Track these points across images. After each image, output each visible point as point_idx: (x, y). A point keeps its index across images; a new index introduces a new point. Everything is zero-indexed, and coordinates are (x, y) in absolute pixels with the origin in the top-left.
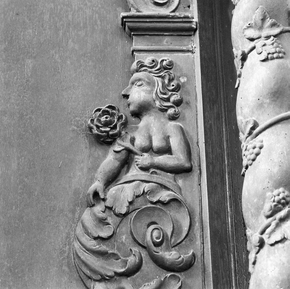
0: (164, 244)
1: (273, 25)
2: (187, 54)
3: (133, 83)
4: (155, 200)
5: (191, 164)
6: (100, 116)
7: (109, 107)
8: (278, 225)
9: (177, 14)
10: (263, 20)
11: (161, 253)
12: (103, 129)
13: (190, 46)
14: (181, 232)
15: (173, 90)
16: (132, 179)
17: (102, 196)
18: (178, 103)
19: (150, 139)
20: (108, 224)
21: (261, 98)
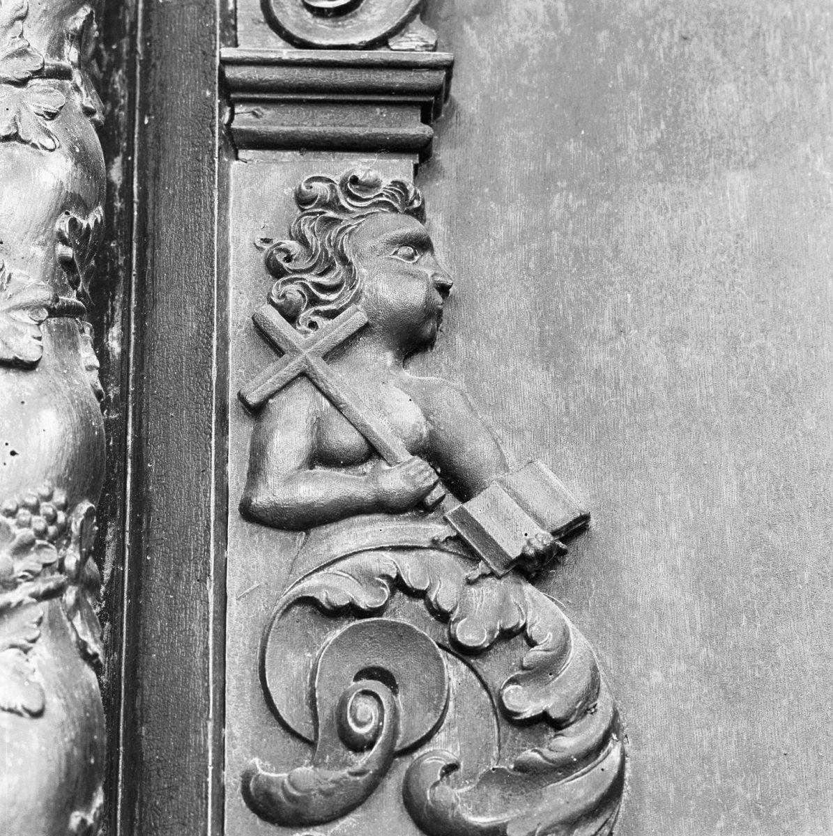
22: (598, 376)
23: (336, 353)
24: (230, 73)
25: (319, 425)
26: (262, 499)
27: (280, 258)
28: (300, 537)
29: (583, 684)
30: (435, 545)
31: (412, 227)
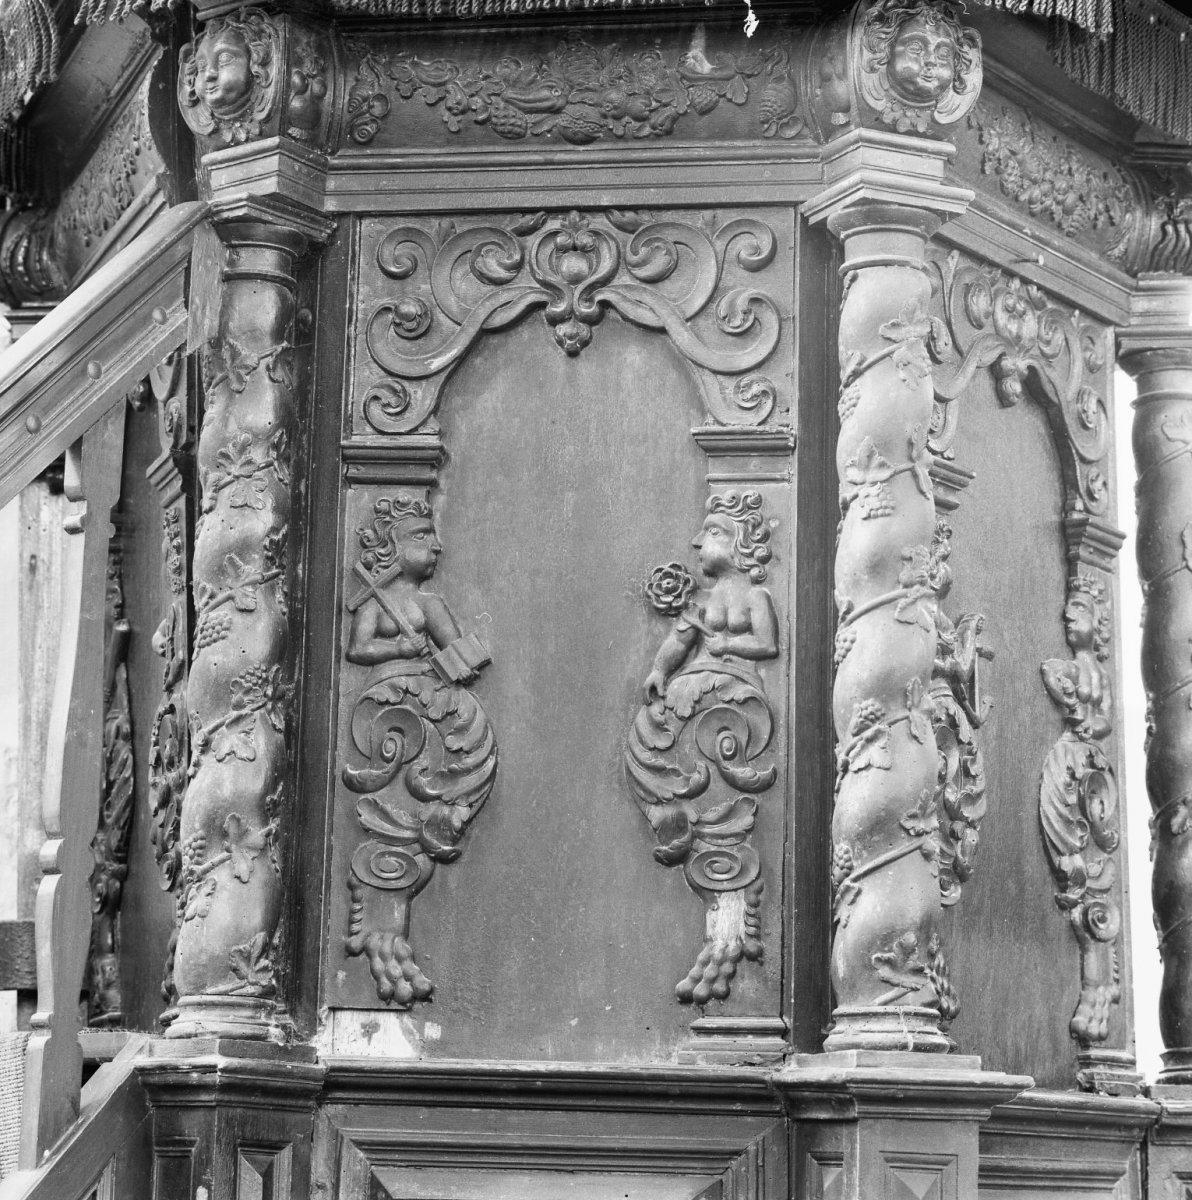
0: (737, 758)
1: (882, 465)
2: (781, 484)
3: (707, 529)
4: (727, 698)
5: (778, 649)
6: (661, 579)
7: (673, 566)
8: (863, 747)
9: (766, 428)
10: (870, 457)
11: (732, 769)
12: (664, 599)
13: (786, 472)
14: (758, 739)
15: (758, 541)
16: (702, 668)
17: (660, 691)
18: (764, 560)
19: (725, 613)
20: (667, 730)
21: (858, 573)
22: (501, 591)
23: (387, 584)
24: (347, 452)
25: (379, 617)
26: (353, 653)
27: (365, 541)
28: (370, 669)
29: (479, 735)
30: (423, 674)
31: (424, 524)
